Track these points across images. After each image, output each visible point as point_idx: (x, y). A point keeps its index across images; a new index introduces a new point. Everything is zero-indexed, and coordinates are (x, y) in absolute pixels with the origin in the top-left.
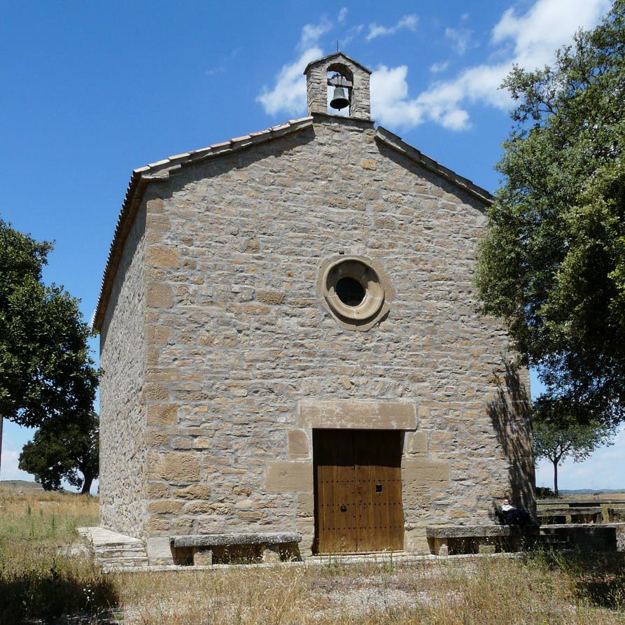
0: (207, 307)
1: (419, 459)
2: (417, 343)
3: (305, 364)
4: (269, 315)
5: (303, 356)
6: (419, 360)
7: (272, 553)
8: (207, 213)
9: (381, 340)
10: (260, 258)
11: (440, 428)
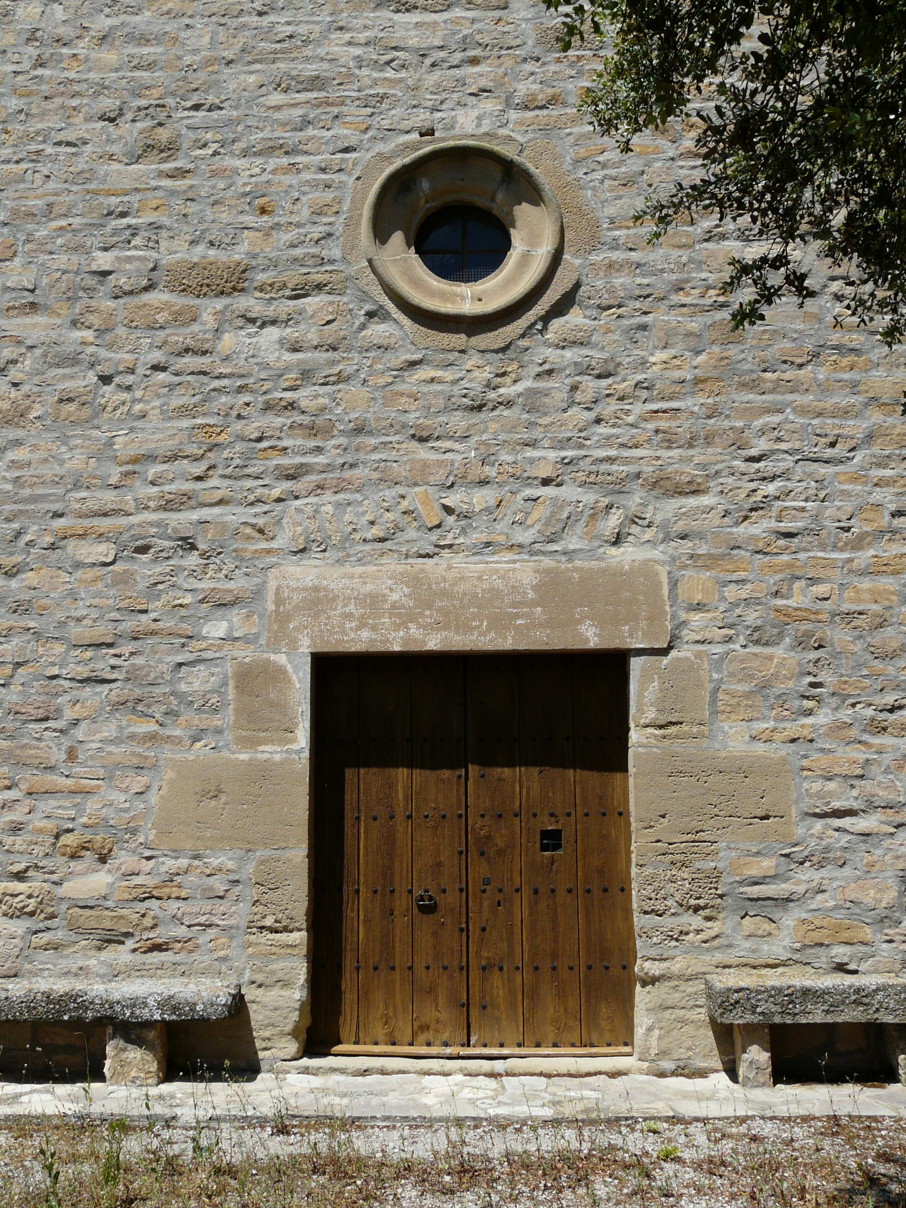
0: (19, 321)
1: (677, 746)
2: (677, 374)
3: (299, 460)
4: (196, 328)
5: (293, 437)
6: (683, 426)
7: (135, 1054)
8: (39, 72)
9: (550, 372)
10: (182, 173)
11: (757, 642)
